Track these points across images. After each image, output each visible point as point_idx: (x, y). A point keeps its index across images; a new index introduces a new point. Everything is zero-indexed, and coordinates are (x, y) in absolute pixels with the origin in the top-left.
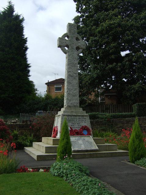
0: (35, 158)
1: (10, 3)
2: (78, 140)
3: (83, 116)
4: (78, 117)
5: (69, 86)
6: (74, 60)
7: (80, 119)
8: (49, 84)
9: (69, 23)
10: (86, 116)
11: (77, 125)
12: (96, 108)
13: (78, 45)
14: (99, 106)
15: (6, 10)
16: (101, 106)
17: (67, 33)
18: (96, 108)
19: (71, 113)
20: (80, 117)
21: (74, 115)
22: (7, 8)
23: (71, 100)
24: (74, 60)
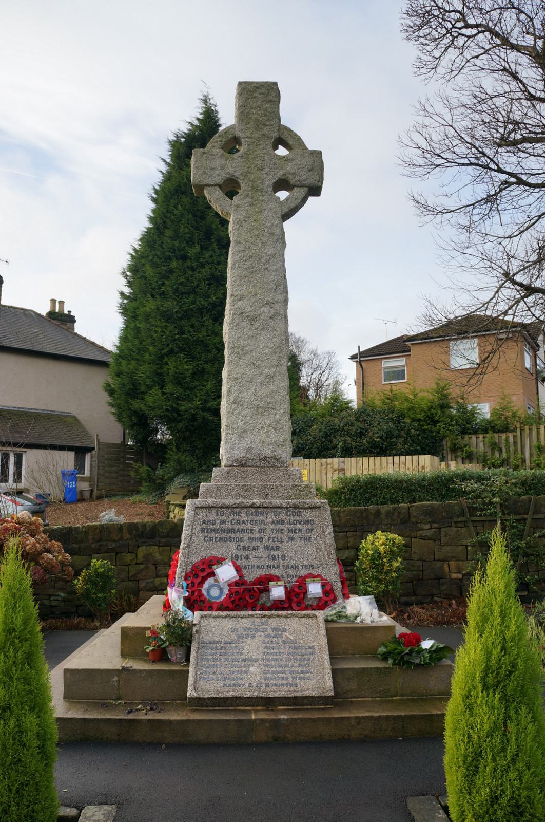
0: (350, 595)
1: (205, 101)
2: (250, 633)
3: (296, 507)
4: (271, 517)
5: (238, 365)
6: (264, 244)
7: (282, 522)
8: (363, 358)
9: (240, 84)
10: (314, 508)
11: (262, 552)
12: (511, 439)
13: (281, 172)
14: (522, 430)
15: (197, 126)
16: (530, 430)
17: (234, 125)
18: (511, 439)
19: (238, 496)
20: (283, 516)
21: (252, 506)
22: (198, 119)
23: (245, 431)
24: (264, 244)
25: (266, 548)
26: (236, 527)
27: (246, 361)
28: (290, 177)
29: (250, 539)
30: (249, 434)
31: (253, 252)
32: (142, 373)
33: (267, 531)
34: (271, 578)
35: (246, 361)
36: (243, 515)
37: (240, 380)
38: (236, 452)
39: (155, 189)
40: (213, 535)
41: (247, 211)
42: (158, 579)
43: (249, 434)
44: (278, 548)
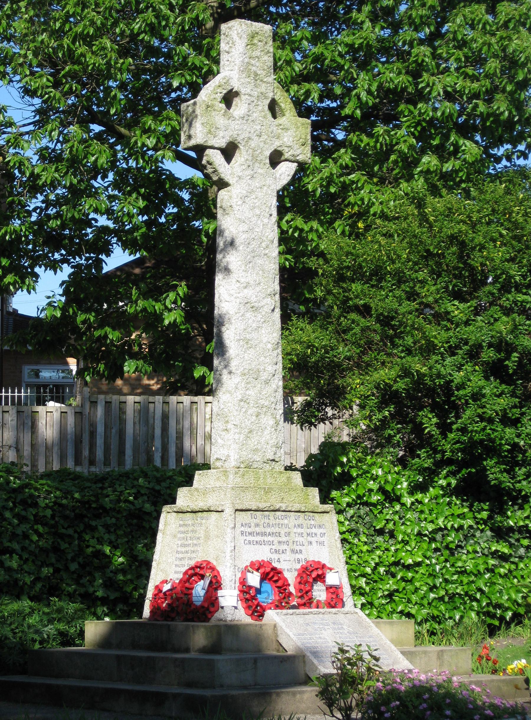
25: (292, 551)
26: (268, 530)
27: (250, 356)
28: (286, 149)
29: (280, 542)
30: (255, 435)
31: (256, 234)
32: (94, 403)
33: (291, 535)
34: (243, 582)
35: (250, 356)
36: (272, 518)
37: (247, 376)
38: (244, 453)
39: (233, 89)
40: (251, 538)
41: (249, 185)
42: (440, 595)
43: (255, 435)
44: (301, 551)
